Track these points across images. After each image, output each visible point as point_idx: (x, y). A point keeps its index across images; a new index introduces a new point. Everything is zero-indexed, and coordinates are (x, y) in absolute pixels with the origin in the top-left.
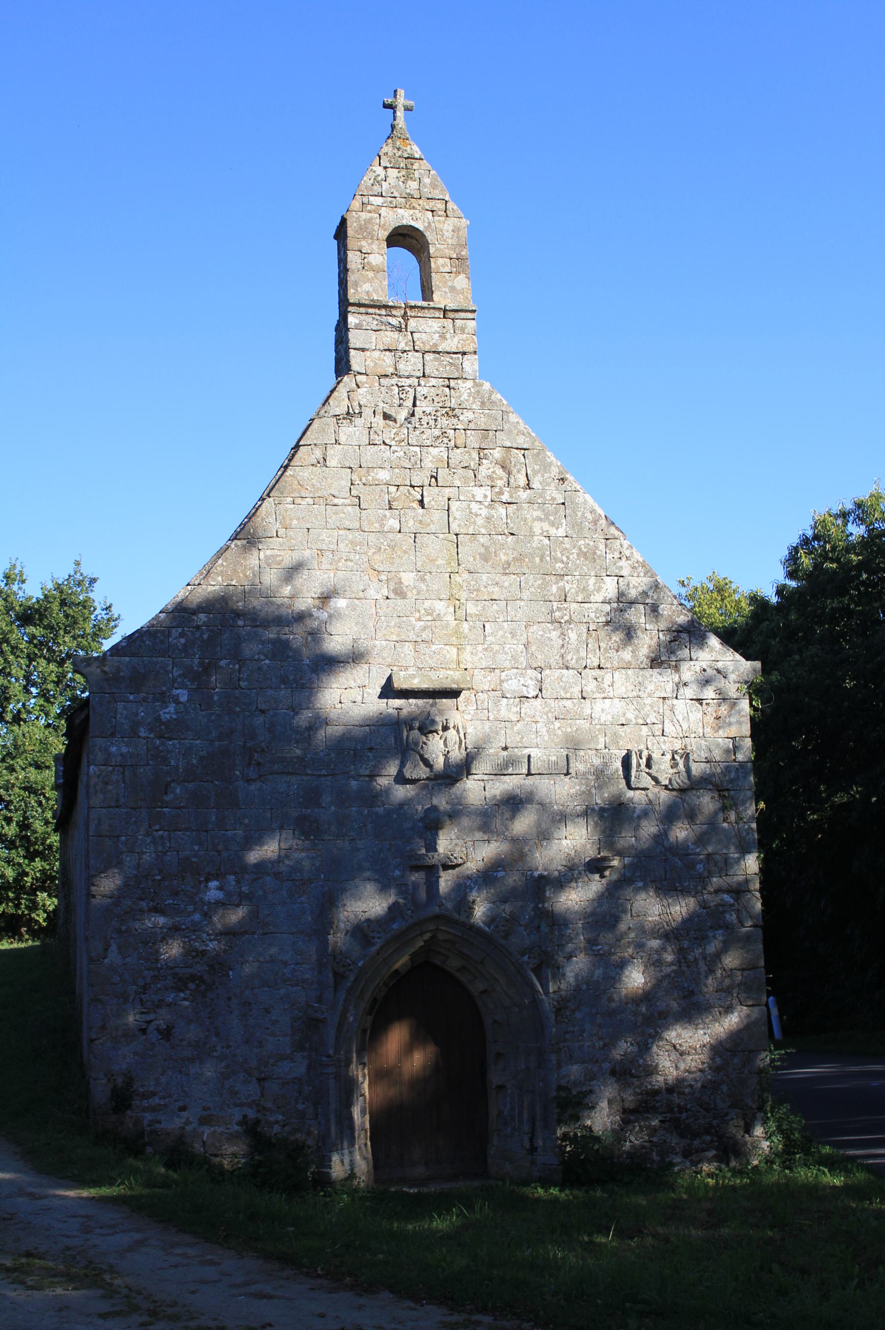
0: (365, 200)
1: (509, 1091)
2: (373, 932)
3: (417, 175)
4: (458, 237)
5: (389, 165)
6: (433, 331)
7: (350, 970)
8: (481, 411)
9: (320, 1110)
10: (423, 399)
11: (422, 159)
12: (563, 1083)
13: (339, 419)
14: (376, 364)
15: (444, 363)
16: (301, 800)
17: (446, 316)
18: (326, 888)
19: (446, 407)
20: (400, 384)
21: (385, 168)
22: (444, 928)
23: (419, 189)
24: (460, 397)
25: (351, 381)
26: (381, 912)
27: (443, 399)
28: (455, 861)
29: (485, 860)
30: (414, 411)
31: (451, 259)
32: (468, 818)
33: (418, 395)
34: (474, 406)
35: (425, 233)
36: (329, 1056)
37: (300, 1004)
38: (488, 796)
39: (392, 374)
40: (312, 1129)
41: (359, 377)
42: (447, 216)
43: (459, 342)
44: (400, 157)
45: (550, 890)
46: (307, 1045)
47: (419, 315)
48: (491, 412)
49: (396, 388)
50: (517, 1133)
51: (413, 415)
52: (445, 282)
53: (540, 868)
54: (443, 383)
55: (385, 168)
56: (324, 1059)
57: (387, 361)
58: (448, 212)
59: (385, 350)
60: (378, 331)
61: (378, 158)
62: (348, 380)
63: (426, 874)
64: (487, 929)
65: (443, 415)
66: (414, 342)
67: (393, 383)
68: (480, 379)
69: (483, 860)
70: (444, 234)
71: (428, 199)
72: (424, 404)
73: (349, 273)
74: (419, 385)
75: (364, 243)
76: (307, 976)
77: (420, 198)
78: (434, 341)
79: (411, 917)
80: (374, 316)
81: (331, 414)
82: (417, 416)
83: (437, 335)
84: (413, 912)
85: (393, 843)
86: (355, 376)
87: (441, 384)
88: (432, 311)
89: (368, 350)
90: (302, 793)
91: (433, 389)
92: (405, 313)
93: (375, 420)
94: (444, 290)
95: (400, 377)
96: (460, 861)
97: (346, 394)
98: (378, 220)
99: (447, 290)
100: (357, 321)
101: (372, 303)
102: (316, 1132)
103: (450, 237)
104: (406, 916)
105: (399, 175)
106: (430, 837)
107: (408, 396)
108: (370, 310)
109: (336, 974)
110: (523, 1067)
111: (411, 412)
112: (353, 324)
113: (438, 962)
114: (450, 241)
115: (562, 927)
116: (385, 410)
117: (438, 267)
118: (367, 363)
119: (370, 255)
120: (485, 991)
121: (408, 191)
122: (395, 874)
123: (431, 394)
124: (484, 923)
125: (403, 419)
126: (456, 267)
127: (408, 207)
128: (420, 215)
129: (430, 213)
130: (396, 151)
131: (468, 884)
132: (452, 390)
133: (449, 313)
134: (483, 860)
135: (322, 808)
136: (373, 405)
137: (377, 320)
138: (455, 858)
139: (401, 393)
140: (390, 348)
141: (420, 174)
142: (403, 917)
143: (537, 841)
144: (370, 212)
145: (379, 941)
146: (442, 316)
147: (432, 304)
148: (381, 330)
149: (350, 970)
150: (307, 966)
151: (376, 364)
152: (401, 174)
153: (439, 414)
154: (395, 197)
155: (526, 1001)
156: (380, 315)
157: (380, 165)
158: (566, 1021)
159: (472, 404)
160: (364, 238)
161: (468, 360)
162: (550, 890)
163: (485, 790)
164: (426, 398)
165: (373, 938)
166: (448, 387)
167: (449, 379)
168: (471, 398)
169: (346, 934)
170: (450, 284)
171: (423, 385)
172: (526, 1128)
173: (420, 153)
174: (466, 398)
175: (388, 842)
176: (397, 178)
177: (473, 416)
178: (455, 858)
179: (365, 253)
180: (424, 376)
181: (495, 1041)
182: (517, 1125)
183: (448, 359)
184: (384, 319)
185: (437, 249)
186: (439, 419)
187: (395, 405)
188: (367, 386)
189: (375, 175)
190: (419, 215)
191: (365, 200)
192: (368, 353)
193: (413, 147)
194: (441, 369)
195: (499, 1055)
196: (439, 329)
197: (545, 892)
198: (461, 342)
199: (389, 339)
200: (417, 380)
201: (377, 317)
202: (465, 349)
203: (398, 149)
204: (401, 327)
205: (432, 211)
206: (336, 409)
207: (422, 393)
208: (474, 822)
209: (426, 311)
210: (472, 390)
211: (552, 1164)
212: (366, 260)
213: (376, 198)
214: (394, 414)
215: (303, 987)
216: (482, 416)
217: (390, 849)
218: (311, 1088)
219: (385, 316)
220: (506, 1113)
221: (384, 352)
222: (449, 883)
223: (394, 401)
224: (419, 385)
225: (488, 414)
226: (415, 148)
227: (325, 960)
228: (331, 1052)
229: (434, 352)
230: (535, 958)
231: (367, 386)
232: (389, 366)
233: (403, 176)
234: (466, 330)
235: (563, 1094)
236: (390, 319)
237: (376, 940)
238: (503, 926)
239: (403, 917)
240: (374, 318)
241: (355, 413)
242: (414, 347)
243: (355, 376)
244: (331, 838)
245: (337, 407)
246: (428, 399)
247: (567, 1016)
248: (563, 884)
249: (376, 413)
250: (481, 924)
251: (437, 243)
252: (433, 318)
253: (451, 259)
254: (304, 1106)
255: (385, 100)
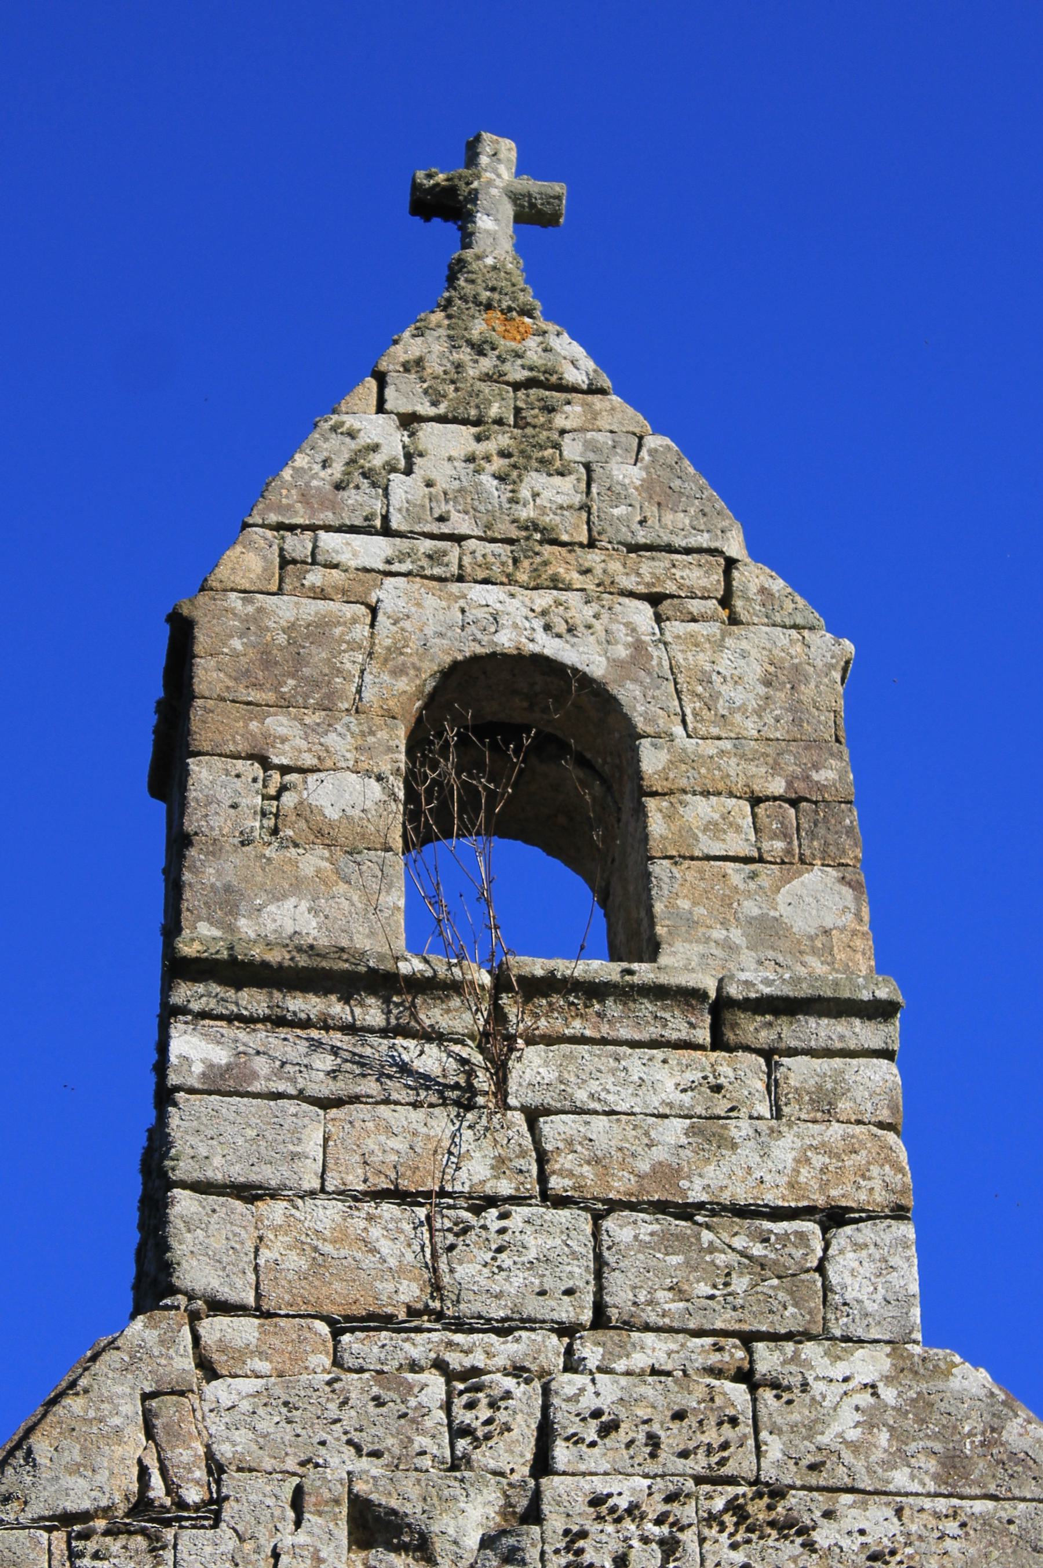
0: (298, 545)
3: (572, 450)
4: (795, 708)
5: (425, 409)
6: (655, 1103)
8: (942, 1505)
10: (592, 1435)
11: (602, 392)
13: (85, 1536)
14: (319, 1262)
15: (721, 1259)
17: (730, 1037)
19: (731, 1481)
20: (456, 1361)
21: (409, 421)
23: (586, 508)
24: (812, 1428)
25: (168, 1342)
26: (195, 648)
27: (712, 1436)
30: (537, 1497)
31: (755, 801)
33: (564, 1419)
34: (900, 1478)
35: (613, 689)
39: (413, 1312)
41: (213, 1328)
42: (734, 620)
43: (803, 1160)
44: (487, 378)
47: (577, 1027)
48: (1006, 1511)
49: (435, 1385)
51: (533, 1515)
52: (727, 902)
54: (714, 1358)
55: (409, 421)
57: (385, 1247)
58: (739, 604)
59: (379, 1196)
60: (338, 1102)
61: (371, 383)
62: (152, 1336)
65: (712, 1519)
66: (542, 1158)
67: (415, 1353)
68: (928, 1342)
70: (715, 696)
71: (634, 548)
72: (597, 1459)
73: (192, 852)
74: (572, 1365)
75: (279, 724)
77: (592, 544)
78: (659, 1154)
80: (314, 1034)
81: (37, 1509)
82: (555, 1522)
83: (679, 1125)
86: (194, 1317)
87: (699, 1362)
88: (646, 1007)
89: (274, 1194)
91: (651, 1389)
92: (498, 1015)
93: (302, 1538)
94: (718, 934)
95: (459, 1325)
97: (133, 1408)
98: (361, 631)
99: (737, 936)
100: (221, 1056)
101: (303, 961)
103: (753, 704)
105: (480, 448)
107: (502, 1416)
108: (300, 1004)
111: (522, 1504)
112: (198, 1068)
114: (750, 726)
116: (360, 1487)
117: (687, 833)
118: (265, 1254)
119: (311, 778)
121: (526, 513)
123: (643, 1413)
125: (472, 1541)
126: (786, 836)
127: (522, 577)
128: (589, 611)
129: (646, 610)
130: (465, 355)
132: (767, 1395)
133: (742, 1017)
136: (291, 1465)
137: (335, 1051)
139: (459, 1402)
140: (405, 1184)
141: (591, 446)
144: (321, 594)
146: (704, 1035)
147: (644, 972)
148: (355, 1099)
151: (319, 1262)
152: (491, 446)
153: (687, 1512)
154: (458, 539)
156: (350, 1029)
157: (381, 409)
159: (889, 1465)
160: (284, 704)
161: (858, 1247)
164: (608, 1429)
166: (745, 1376)
167: (748, 1339)
168: (883, 1437)
170: (750, 908)
171: (592, 1363)
173: (589, 364)
174: (853, 1435)
176: (470, 459)
177: (894, 1526)
179: (285, 770)
180: (600, 1320)
183: (739, 1242)
184: (378, 1048)
185: (683, 759)
186: (688, 1537)
187: (426, 1462)
188: (263, 1366)
189: (353, 445)
190: (580, 611)
191: (298, 545)
192: (275, 1211)
193: (554, 342)
194: (704, 1289)
196: (687, 1098)
198: (818, 1160)
199: (398, 1144)
200: (555, 1343)
201: (337, 1038)
202: (841, 1194)
203: (479, 349)
204: (471, 1090)
205: (655, 599)
206: (67, 1480)
207: (589, 1402)
209: (613, 1008)
210: (889, 1394)
212: (289, 799)
213: (358, 541)
214: (412, 1509)
216: (952, 1527)
219: (384, 1032)
221: (368, 1207)
223: (421, 1441)
224: (572, 1365)
225: (986, 1521)
226: (566, 346)
229: (661, 1207)
231: (263, 1366)
232: (397, 1273)
233: (504, 454)
234: (844, 1106)
236: (408, 1049)
240: (316, 1045)
241: (181, 1504)
242: (543, 1178)
243: (194, 1317)
245: (74, 1469)
246: (622, 1435)
249: (309, 1501)
251: (678, 730)
252: (654, 1044)
253: (755, 801)
255: (420, 175)
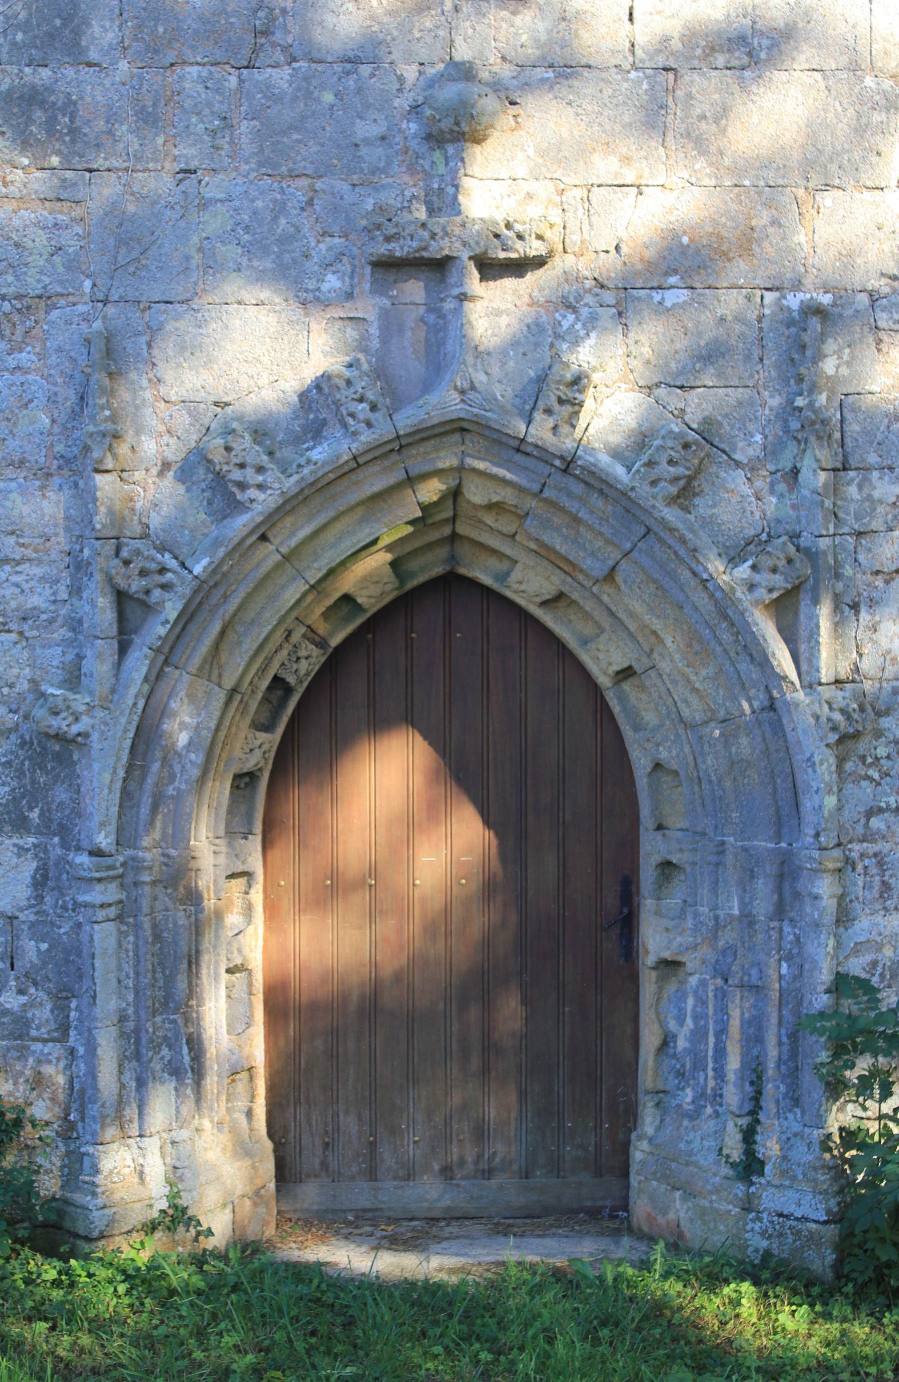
1: (693, 981)
2: (242, 466)
7: (165, 587)
9: (73, 1014)
12: (856, 967)
16: (20, 36)
18: (97, 325)
22: (481, 465)
28: (519, 245)
29: (625, 249)
32: (571, 111)
36: (97, 853)
37: (11, 686)
38: (641, 40)
40: (48, 1070)
45: (839, 353)
46: (35, 815)
50: (709, 1110)
53: (808, 281)
56: (83, 859)
63: (427, 288)
64: (619, 471)
69: (617, 248)
76: (36, 601)
79: (369, 425)
84: (374, 408)
85: (318, 185)
90: (23, 15)
96: (535, 248)
102: (61, 1080)
104: (350, 421)
106: (442, 169)
109: (121, 597)
110: (736, 912)
113: (486, 579)
115: (875, 474)
120: (627, 673)
122: (325, 287)
124: (616, 454)
131: (566, 324)
134: (617, 248)
135: (90, 65)
138: (520, 237)
142: (345, 426)
143: (801, 192)
145: (261, 496)
149: (165, 587)
150: (38, 571)
155: (745, 705)
158: (876, 776)
162: (839, 353)
163: (631, 19)
165: (242, 486)
169: (161, 474)
172: (732, 1097)
175: (304, 182)
178: (520, 237)
181: (660, 827)
182: (711, 1083)
195: (667, 867)
197: (819, 356)
208: (590, 125)
211: (805, 1219)
215: (21, 633)
217: (310, 203)
218: (44, 946)
220: (682, 1044)
222: (504, 320)
227: (86, 552)
228: (104, 840)
230: (774, 570)
235: (848, 1005)
237: (252, 493)
238: (671, 462)
239: (345, 426)
244: (115, 163)
247: (877, 759)
248: (883, 335)
250: (604, 459)
254: (23, 999)
